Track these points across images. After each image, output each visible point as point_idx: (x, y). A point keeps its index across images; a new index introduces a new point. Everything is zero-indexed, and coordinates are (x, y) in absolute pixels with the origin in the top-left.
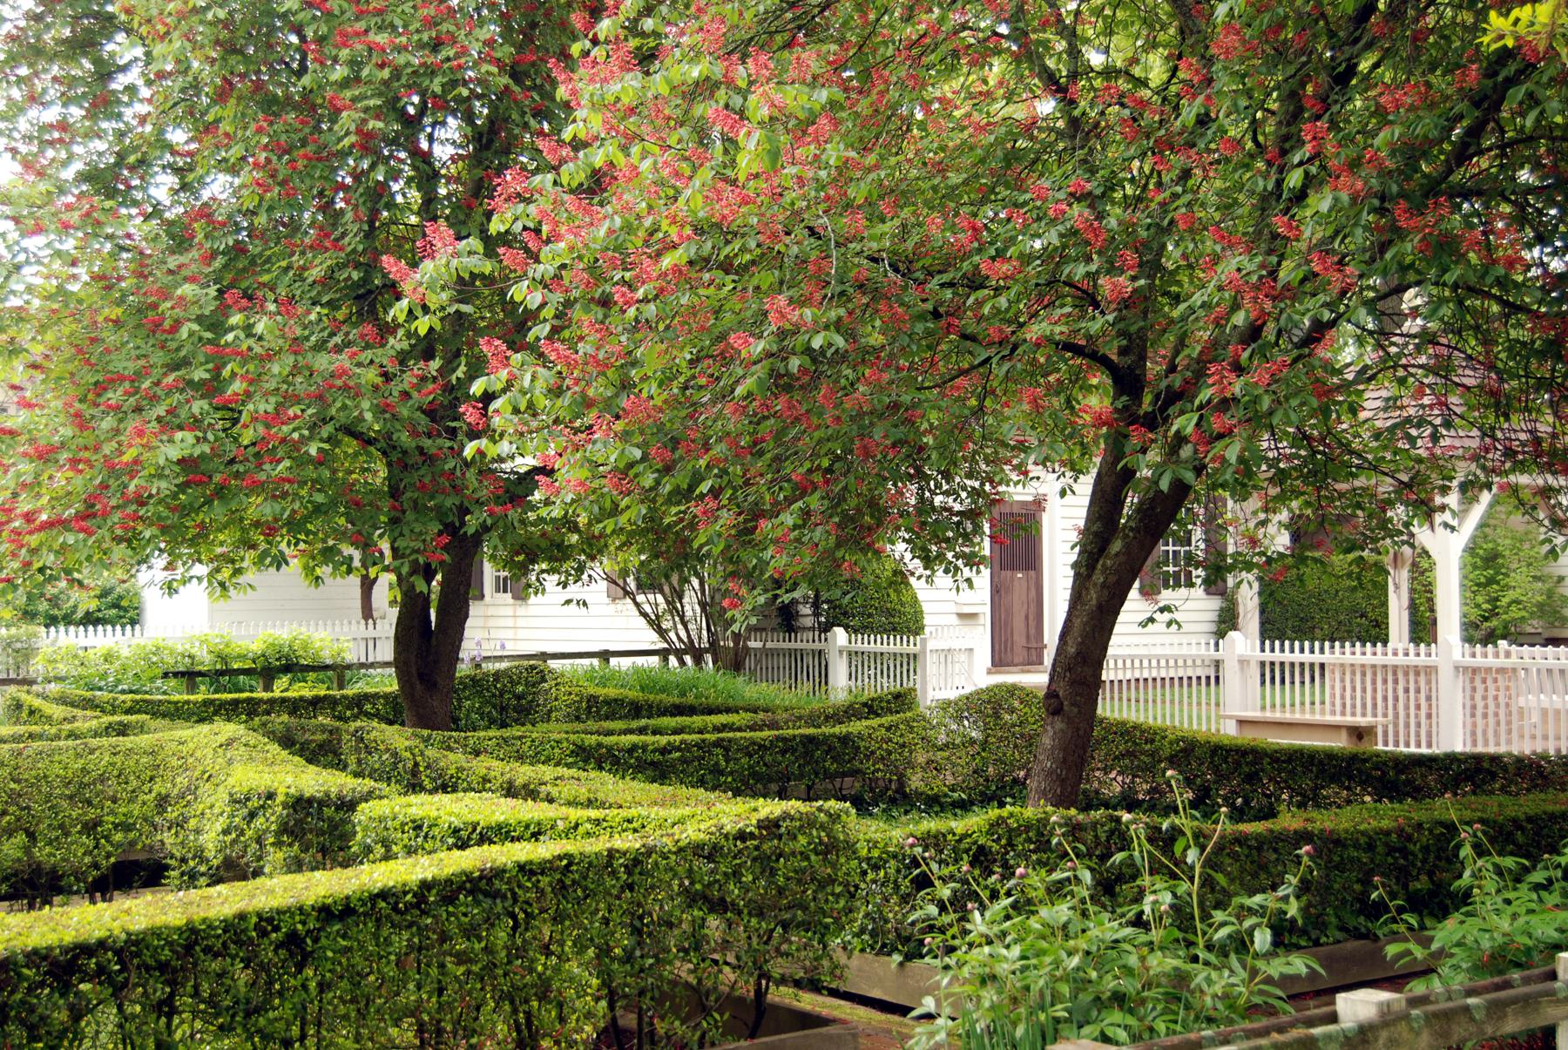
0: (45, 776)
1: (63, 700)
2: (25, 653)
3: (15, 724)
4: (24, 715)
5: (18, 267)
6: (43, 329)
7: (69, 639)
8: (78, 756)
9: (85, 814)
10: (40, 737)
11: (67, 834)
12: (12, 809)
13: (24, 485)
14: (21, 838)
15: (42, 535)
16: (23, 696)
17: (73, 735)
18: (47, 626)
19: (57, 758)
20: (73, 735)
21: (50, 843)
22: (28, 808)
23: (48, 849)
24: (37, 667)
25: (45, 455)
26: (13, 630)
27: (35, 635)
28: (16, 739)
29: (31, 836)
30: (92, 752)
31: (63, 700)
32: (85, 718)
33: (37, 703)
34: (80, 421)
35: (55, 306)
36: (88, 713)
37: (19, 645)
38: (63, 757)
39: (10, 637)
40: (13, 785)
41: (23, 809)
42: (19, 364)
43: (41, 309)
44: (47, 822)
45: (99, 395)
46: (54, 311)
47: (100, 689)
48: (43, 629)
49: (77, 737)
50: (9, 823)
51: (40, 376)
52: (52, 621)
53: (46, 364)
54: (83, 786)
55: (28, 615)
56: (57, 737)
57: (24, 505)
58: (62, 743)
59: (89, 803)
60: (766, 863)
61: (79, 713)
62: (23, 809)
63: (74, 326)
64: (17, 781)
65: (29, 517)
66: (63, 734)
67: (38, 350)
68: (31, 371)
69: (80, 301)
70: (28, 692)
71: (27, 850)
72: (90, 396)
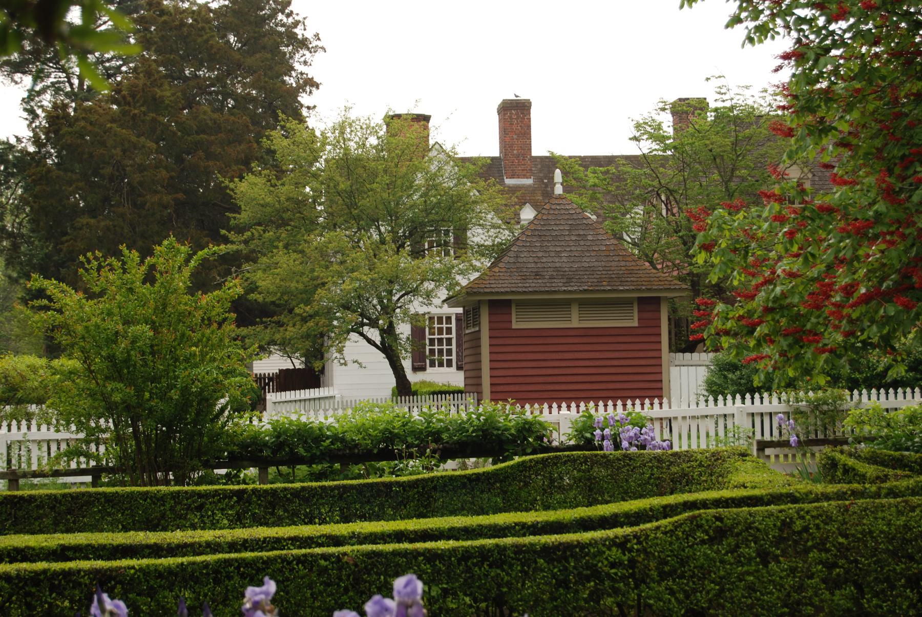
0: (871, 532)
1: (873, 459)
2: (833, 415)
3: (830, 482)
4: (839, 474)
5: (827, 50)
6: (849, 108)
7: (871, 401)
8: (900, 513)
9: (909, 569)
10: (862, 494)
11: (892, 587)
12: (841, 562)
13: (842, 261)
14: (851, 589)
15: (863, 308)
16: (838, 456)
17: (892, 493)
18: (851, 390)
19: (880, 515)
20: (892, 493)
21: (876, 595)
22: (856, 561)
23: (875, 601)
24: (846, 426)
25: (861, 231)
26: (820, 394)
27: (841, 398)
28: (840, 496)
29: (859, 587)
30: (913, 509)
31: (873, 459)
32: (896, 477)
33: (851, 462)
34: (889, 194)
35: (859, 86)
36: (899, 472)
37: (825, 408)
38: (886, 514)
39: (817, 400)
40: (841, 540)
41: (851, 562)
42: (828, 142)
43: (845, 88)
44: (874, 575)
45: (906, 168)
46: (858, 91)
47: (907, 449)
48: (847, 392)
49: (896, 496)
50: (838, 575)
51: (847, 153)
52: (853, 385)
53: (854, 141)
54: (906, 542)
55: (835, 380)
56: (877, 495)
57: (842, 278)
58: (884, 501)
59: (911, 558)
60: (432, 482)
61: (891, 472)
62: (851, 562)
63: (877, 103)
64: (846, 536)
65: (849, 290)
66: (884, 492)
67: (845, 127)
68: (841, 149)
69: (883, 78)
70: (842, 452)
71: (857, 601)
72: (897, 170)
